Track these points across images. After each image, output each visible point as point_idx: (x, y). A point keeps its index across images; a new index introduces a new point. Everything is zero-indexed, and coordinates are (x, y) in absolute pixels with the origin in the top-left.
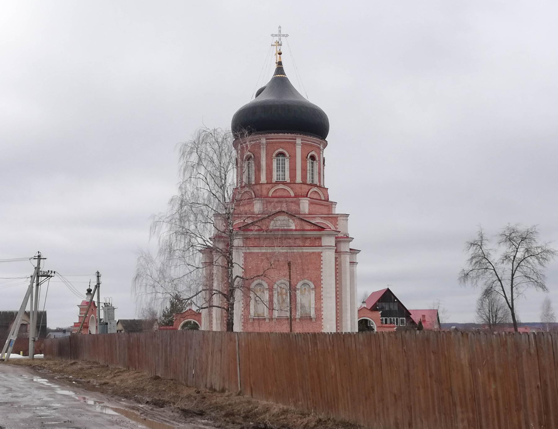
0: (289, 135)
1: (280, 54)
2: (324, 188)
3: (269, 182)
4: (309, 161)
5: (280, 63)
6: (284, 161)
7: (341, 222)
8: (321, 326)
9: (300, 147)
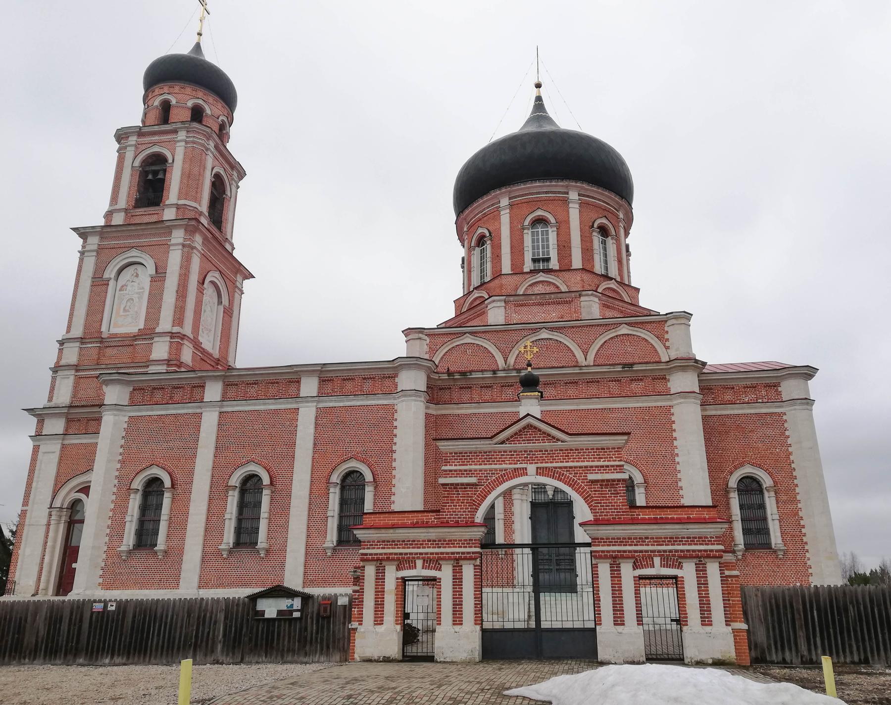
1: (538, 86)
2: (629, 286)
3: (517, 271)
4: (597, 239)
5: (539, 99)
6: (547, 234)
7: (673, 332)
8: (804, 570)
9: (577, 206)
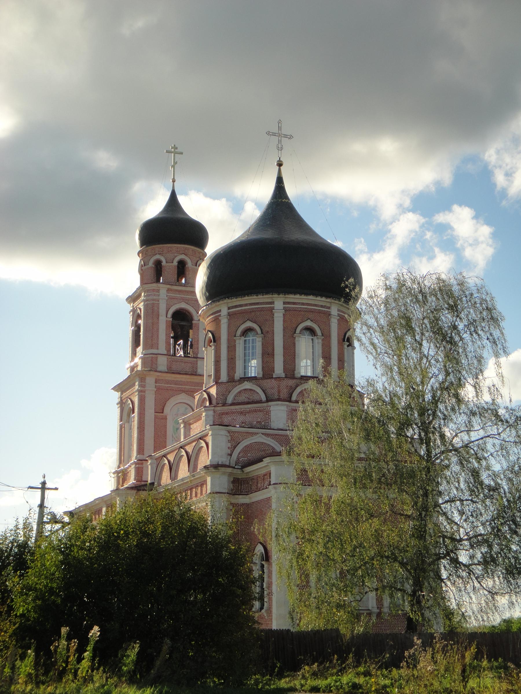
0: (324, 299)
5: (280, 181)
9: (336, 321)
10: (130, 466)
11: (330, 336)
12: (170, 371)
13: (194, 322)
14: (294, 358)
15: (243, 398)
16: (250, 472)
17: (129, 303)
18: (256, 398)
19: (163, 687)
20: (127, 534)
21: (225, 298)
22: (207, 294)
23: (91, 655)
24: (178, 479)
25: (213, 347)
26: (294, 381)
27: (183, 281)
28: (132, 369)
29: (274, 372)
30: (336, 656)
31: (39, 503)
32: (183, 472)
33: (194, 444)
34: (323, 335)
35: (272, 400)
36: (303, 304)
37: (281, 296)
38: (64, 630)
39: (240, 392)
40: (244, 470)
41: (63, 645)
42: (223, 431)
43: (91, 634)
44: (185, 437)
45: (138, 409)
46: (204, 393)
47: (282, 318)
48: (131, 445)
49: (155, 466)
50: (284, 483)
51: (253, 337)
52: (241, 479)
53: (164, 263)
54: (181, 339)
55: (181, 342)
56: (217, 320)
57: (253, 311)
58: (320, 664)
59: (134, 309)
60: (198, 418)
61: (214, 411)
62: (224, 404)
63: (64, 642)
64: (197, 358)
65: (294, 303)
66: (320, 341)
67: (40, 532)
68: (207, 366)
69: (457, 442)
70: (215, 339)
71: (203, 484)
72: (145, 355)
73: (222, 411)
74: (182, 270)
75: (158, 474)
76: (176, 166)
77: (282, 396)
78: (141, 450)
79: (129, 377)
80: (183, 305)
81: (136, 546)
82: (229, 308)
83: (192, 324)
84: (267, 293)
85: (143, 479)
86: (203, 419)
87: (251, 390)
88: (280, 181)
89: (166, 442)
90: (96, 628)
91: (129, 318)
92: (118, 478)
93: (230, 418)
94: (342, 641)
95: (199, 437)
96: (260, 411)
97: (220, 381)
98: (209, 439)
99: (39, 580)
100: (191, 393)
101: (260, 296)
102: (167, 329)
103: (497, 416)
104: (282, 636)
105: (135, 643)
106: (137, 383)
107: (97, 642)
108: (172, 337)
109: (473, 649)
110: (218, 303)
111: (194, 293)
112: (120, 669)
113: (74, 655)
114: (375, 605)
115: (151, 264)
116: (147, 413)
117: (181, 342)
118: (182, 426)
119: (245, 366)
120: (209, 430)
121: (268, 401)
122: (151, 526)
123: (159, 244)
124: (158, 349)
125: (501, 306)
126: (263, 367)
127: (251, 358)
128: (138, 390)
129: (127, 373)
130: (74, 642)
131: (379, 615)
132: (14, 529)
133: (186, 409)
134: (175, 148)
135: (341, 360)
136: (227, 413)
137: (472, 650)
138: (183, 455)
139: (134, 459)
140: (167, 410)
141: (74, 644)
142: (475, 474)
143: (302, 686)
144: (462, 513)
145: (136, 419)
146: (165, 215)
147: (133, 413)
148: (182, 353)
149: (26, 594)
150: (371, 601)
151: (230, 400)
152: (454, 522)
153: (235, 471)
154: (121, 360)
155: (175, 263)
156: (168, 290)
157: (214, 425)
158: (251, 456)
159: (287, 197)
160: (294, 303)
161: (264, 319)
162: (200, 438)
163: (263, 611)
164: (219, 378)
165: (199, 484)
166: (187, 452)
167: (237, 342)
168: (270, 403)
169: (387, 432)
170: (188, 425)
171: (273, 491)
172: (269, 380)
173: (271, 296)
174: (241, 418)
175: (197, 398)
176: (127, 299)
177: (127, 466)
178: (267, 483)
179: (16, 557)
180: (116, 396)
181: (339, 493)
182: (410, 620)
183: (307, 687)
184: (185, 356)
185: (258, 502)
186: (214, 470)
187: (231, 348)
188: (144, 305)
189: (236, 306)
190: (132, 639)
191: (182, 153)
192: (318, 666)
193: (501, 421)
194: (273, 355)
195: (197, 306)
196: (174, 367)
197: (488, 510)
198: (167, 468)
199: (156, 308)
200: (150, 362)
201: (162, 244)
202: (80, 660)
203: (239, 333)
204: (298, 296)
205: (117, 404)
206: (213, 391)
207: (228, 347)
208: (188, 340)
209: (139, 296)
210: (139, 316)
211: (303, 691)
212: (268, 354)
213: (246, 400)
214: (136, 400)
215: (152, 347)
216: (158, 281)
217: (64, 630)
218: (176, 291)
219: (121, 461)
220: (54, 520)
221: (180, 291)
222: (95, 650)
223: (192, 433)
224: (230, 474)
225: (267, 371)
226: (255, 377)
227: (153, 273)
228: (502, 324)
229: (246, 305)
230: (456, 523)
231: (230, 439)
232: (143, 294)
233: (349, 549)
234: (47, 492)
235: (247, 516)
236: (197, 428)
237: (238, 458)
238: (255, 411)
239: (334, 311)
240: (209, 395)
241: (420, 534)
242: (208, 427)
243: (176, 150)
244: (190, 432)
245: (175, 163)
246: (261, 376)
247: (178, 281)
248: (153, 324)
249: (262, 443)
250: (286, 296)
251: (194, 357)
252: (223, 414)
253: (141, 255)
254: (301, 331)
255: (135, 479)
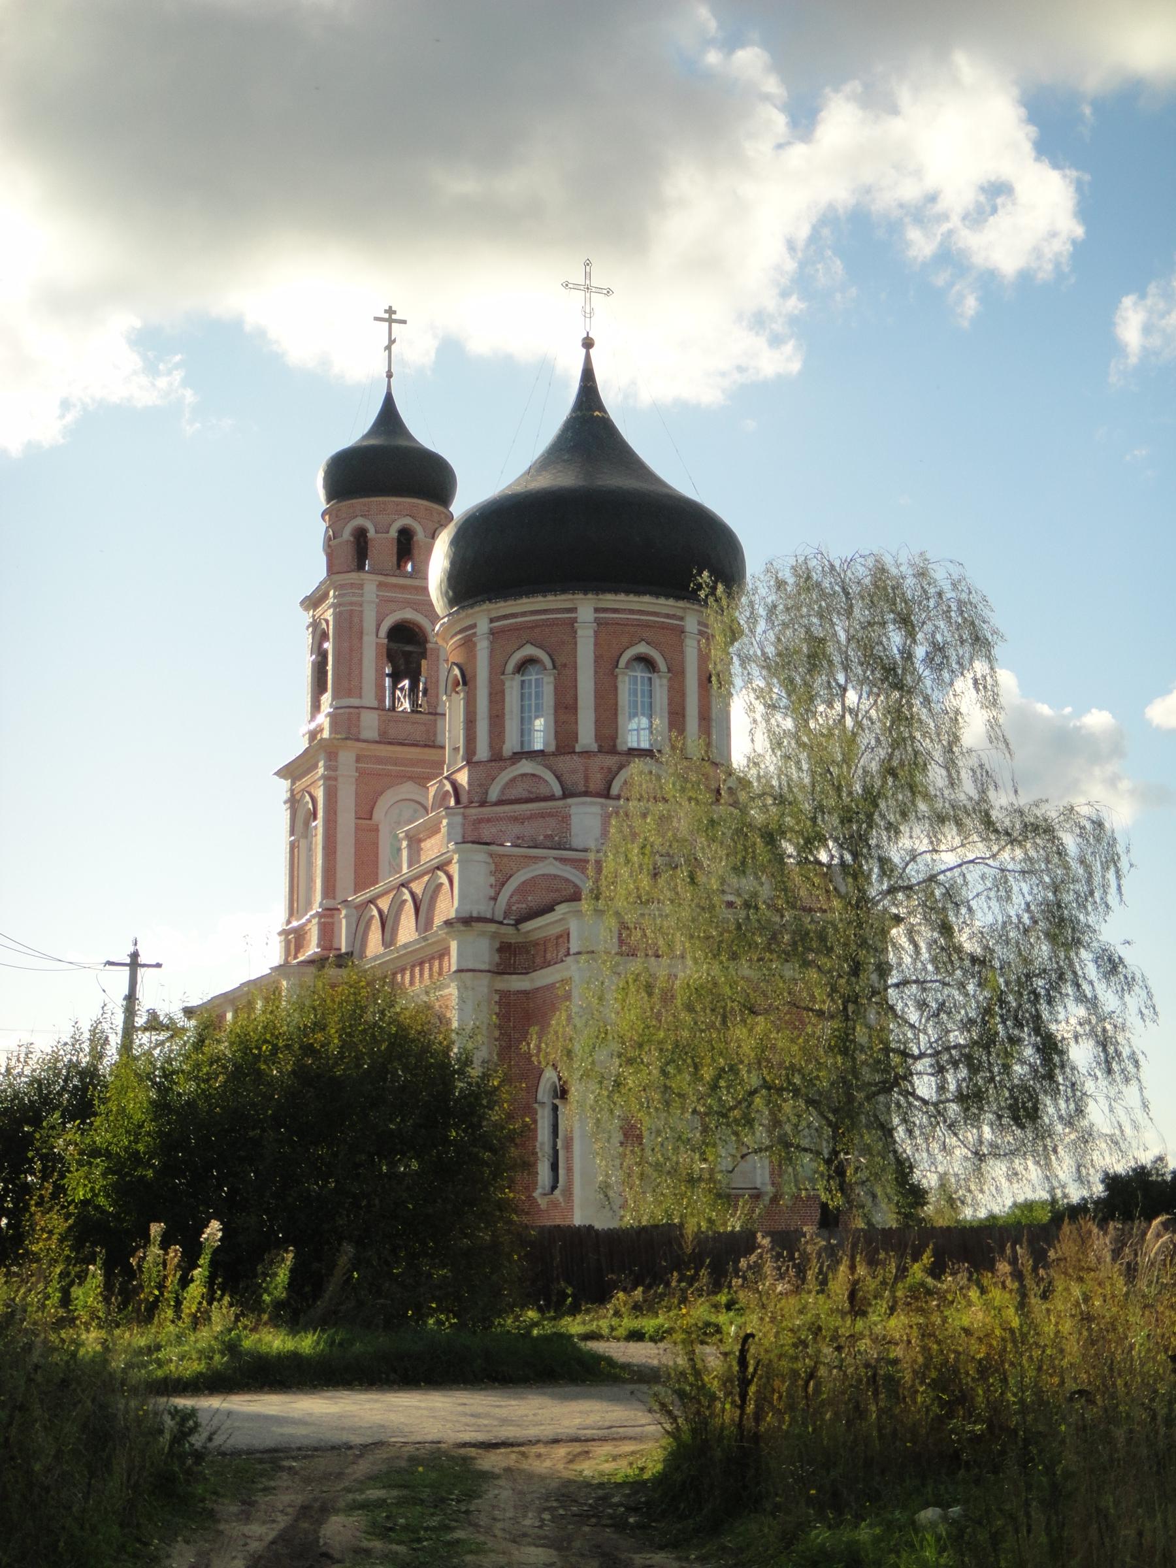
0: (671, 602)
5: (588, 375)
10: (309, 921)
11: (682, 672)
12: (385, 739)
13: (429, 646)
14: (616, 714)
15: (519, 791)
16: (529, 932)
17: (307, 609)
18: (543, 790)
19: (336, 1332)
20: (275, 1050)
21: (484, 601)
22: (451, 593)
23: (207, 1273)
24: (399, 943)
25: (462, 695)
26: (616, 758)
27: (409, 567)
28: (313, 735)
29: (577, 741)
30: (675, 1274)
31: (126, 992)
32: (407, 932)
33: (426, 878)
34: (669, 671)
35: (573, 795)
36: (632, 612)
37: (590, 596)
38: (156, 1229)
39: (513, 780)
40: (520, 927)
41: (156, 1257)
42: (479, 855)
43: (205, 1236)
44: (410, 865)
45: (325, 812)
46: (446, 782)
47: (592, 640)
48: (310, 880)
49: (354, 920)
50: (588, 952)
51: (537, 674)
52: (515, 947)
53: (371, 534)
54: (406, 678)
55: (406, 683)
56: (468, 644)
57: (537, 626)
58: (648, 1288)
59: (314, 620)
60: (434, 830)
61: (465, 816)
62: (483, 804)
63: (155, 1250)
64: (436, 714)
65: (615, 611)
66: (665, 681)
67: (126, 1046)
68: (452, 731)
69: (915, 873)
70: (466, 680)
71: (444, 953)
72: (336, 708)
73: (479, 817)
74: (407, 547)
75: (359, 935)
76: (394, 347)
77: (592, 787)
78: (329, 889)
79: (306, 750)
80: (408, 614)
81: (294, 1072)
82: (492, 621)
83: (425, 649)
84: (564, 591)
85: (335, 946)
86: (444, 830)
87: (533, 775)
88: (588, 375)
89: (377, 874)
90: (215, 1225)
91: (306, 639)
92: (288, 943)
93: (494, 830)
94: (680, 1246)
95: (437, 864)
96: (551, 815)
97: (475, 759)
98: (454, 869)
99: (114, 1136)
100: (422, 781)
101: (550, 598)
102: (377, 657)
103: (988, 822)
104: (583, 1239)
105: (287, 1251)
106: (321, 764)
107: (216, 1251)
108: (388, 675)
109: (927, 1258)
110: (470, 611)
111: (425, 590)
112: (259, 1301)
113: (174, 1275)
114: (767, 1179)
115: (347, 534)
116: (340, 820)
117: (406, 683)
118: (405, 844)
119: (522, 731)
120: (455, 851)
121: (565, 796)
122: (319, 1036)
123: (362, 497)
124: (360, 697)
125: (999, 617)
126: (556, 732)
127: (533, 714)
128: (324, 777)
129: (301, 745)
130: (176, 1251)
131: (775, 1199)
132: (69, 1041)
133: (415, 811)
134: (390, 311)
135: (705, 718)
136: (489, 820)
137: (925, 1261)
138: (405, 901)
139: (316, 908)
140: (378, 814)
141: (175, 1253)
142: (946, 929)
143: (612, 1329)
144: (922, 1005)
145: (320, 830)
146: (372, 442)
147: (315, 818)
148: (406, 705)
149: (90, 1164)
150: (759, 1171)
151: (493, 795)
152: (906, 1022)
153: (503, 930)
154: (292, 719)
155: (393, 533)
156: (381, 585)
157: (464, 842)
158: (533, 901)
159: (601, 408)
160: (615, 611)
161: (557, 642)
162: (438, 868)
163: (557, 1192)
164: (474, 753)
165: (436, 955)
166: (413, 894)
167: (507, 684)
168: (570, 801)
169: (780, 858)
170: (415, 842)
171: (574, 967)
172: (568, 757)
173: (570, 597)
174: (516, 829)
175: (432, 792)
176: (302, 603)
177: (303, 920)
178: (562, 951)
179: (73, 1092)
180: (283, 787)
181: (690, 969)
182: (824, 1206)
183: (621, 1332)
184: (412, 711)
185: (551, 987)
186: (463, 928)
187: (497, 696)
188: (334, 614)
189: (505, 617)
190: (282, 1245)
191: (404, 322)
192: (643, 1292)
193: (996, 831)
194: (576, 709)
195: (434, 618)
196: (392, 733)
197: (969, 998)
198: (376, 924)
199: (356, 620)
200: (345, 722)
201: (369, 496)
202: (185, 1282)
203: (511, 666)
204: (622, 597)
205: (285, 803)
206: (463, 778)
207: (491, 694)
208: (418, 681)
209: (325, 596)
210: (324, 636)
211: (614, 1338)
212: (565, 708)
213: (525, 795)
214: (320, 794)
215: (349, 693)
216: (361, 567)
217: (156, 1229)
218: (395, 586)
219: (292, 912)
220: (154, 1024)
221: (403, 588)
222: (213, 1263)
223: (424, 858)
224: (494, 935)
225: (565, 741)
226: (542, 751)
227: (351, 552)
228: (996, 651)
229: (524, 614)
230: (912, 1026)
231: (493, 867)
232: (331, 593)
233: (707, 1074)
234: (141, 972)
235: (518, 1016)
236: (434, 848)
237: (509, 905)
238: (542, 816)
239: (691, 624)
240: (454, 785)
241: (844, 1045)
242: (451, 846)
243: (394, 317)
244: (419, 855)
245: (392, 342)
246: (552, 748)
247: (399, 566)
248: (351, 650)
249: (555, 876)
250: (601, 597)
251: (430, 713)
252: (480, 821)
253: (327, 517)
254: (628, 663)
255: (319, 946)
